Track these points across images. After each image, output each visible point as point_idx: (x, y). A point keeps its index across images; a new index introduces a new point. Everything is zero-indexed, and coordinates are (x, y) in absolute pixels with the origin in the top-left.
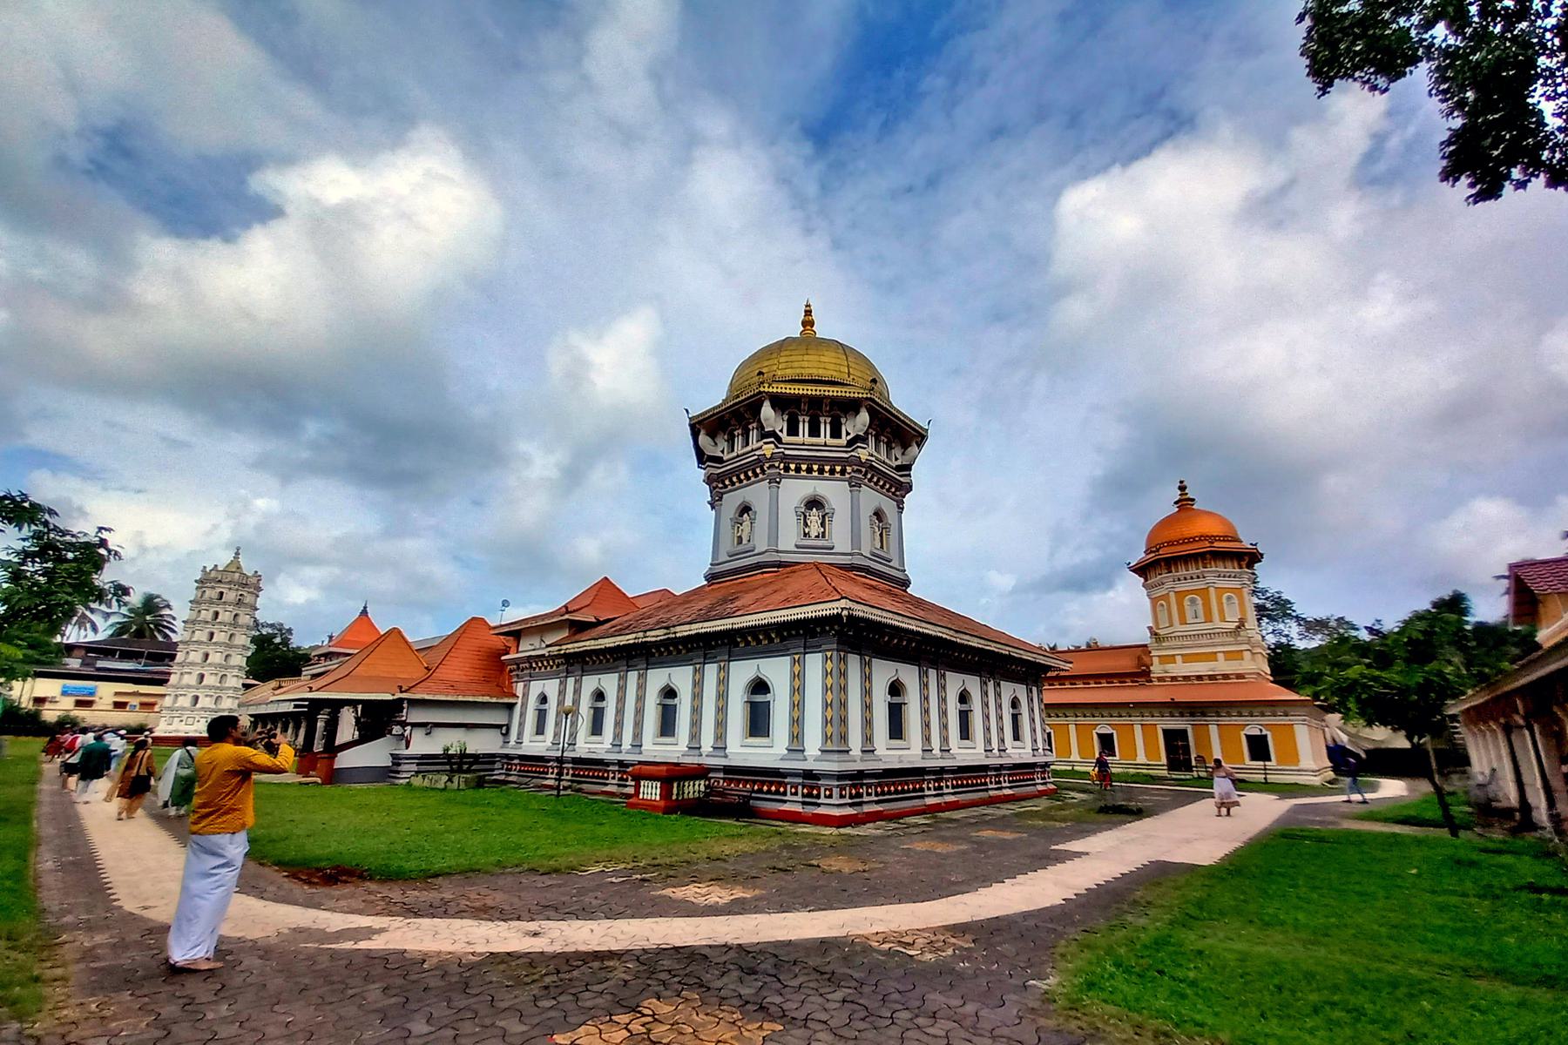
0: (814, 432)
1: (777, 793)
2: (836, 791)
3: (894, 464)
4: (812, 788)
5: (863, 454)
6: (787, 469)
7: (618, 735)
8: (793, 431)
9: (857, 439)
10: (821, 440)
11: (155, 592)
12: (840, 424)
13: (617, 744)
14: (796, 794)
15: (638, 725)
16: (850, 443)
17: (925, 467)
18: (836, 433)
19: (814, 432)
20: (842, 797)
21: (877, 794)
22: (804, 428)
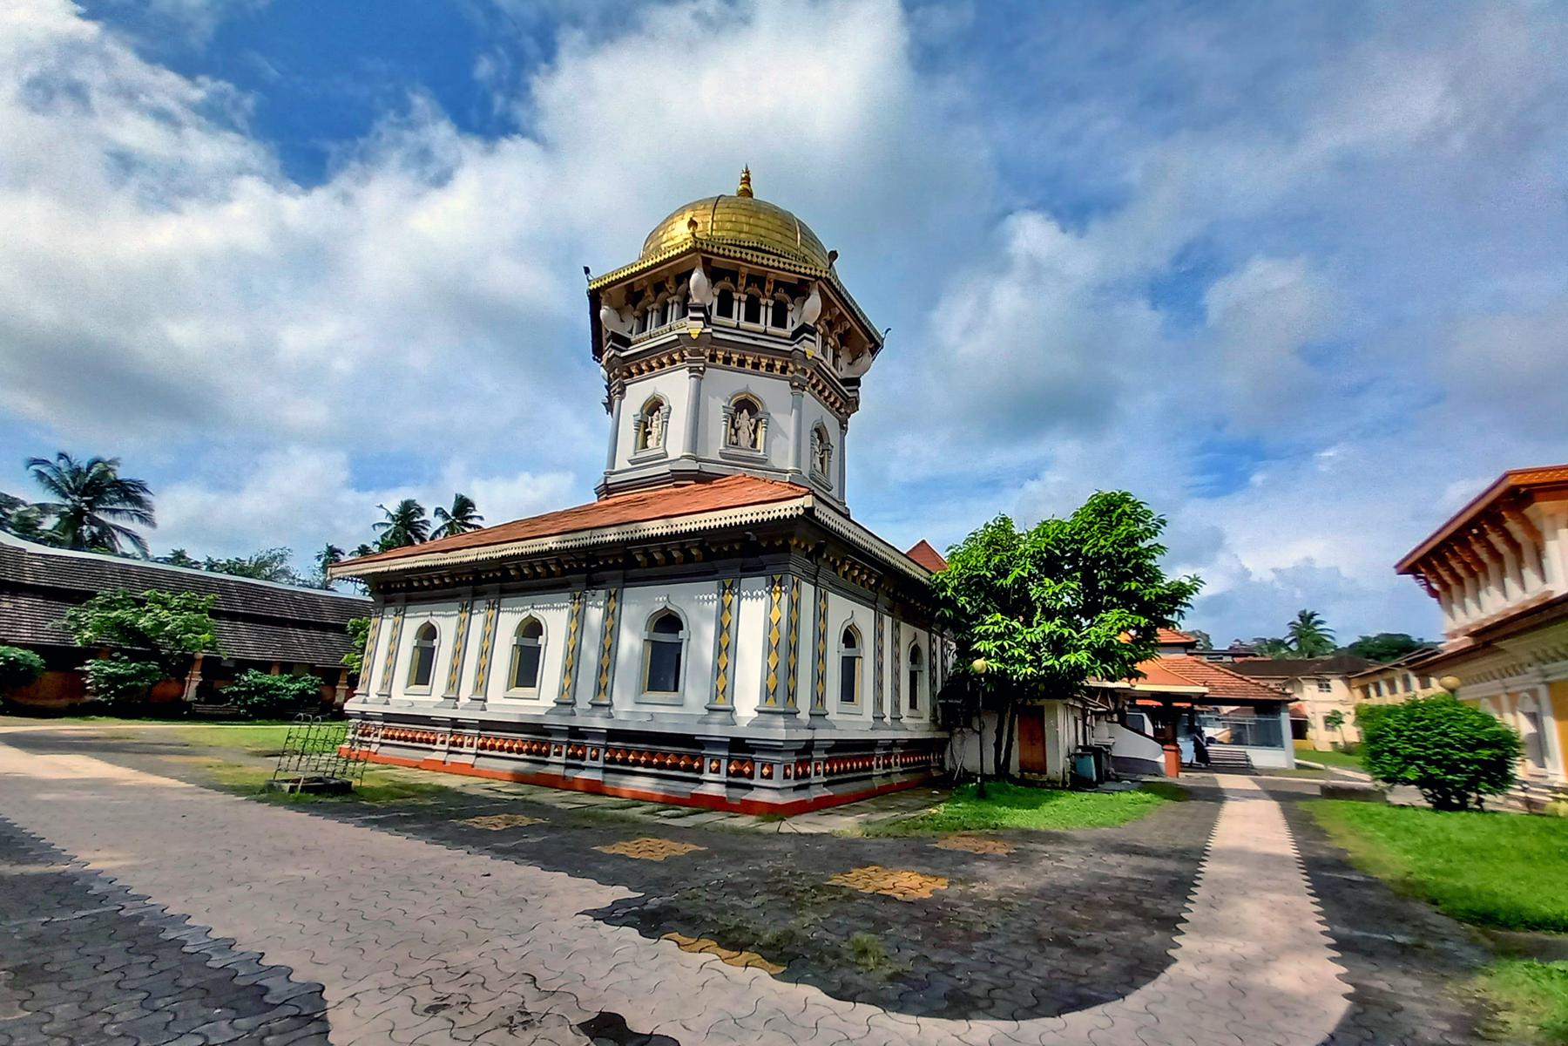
0: (752, 316)
1: (688, 768)
2: (778, 771)
3: (841, 375)
4: (543, 743)
5: (812, 348)
6: (713, 358)
7: (454, 684)
8: (725, 310)
9: (804, 328)
10: (760, 327)
11: (1137, 495)
12: (786, 311)
13: (453, 697)
14: (596, 758)
15: (484, 670)
16: (795, 335)
17: (878, 380)
18: (780, 321)
19: (752, 316)
20: (786, 777)
21: (797, 777)
22: (739, 309)
